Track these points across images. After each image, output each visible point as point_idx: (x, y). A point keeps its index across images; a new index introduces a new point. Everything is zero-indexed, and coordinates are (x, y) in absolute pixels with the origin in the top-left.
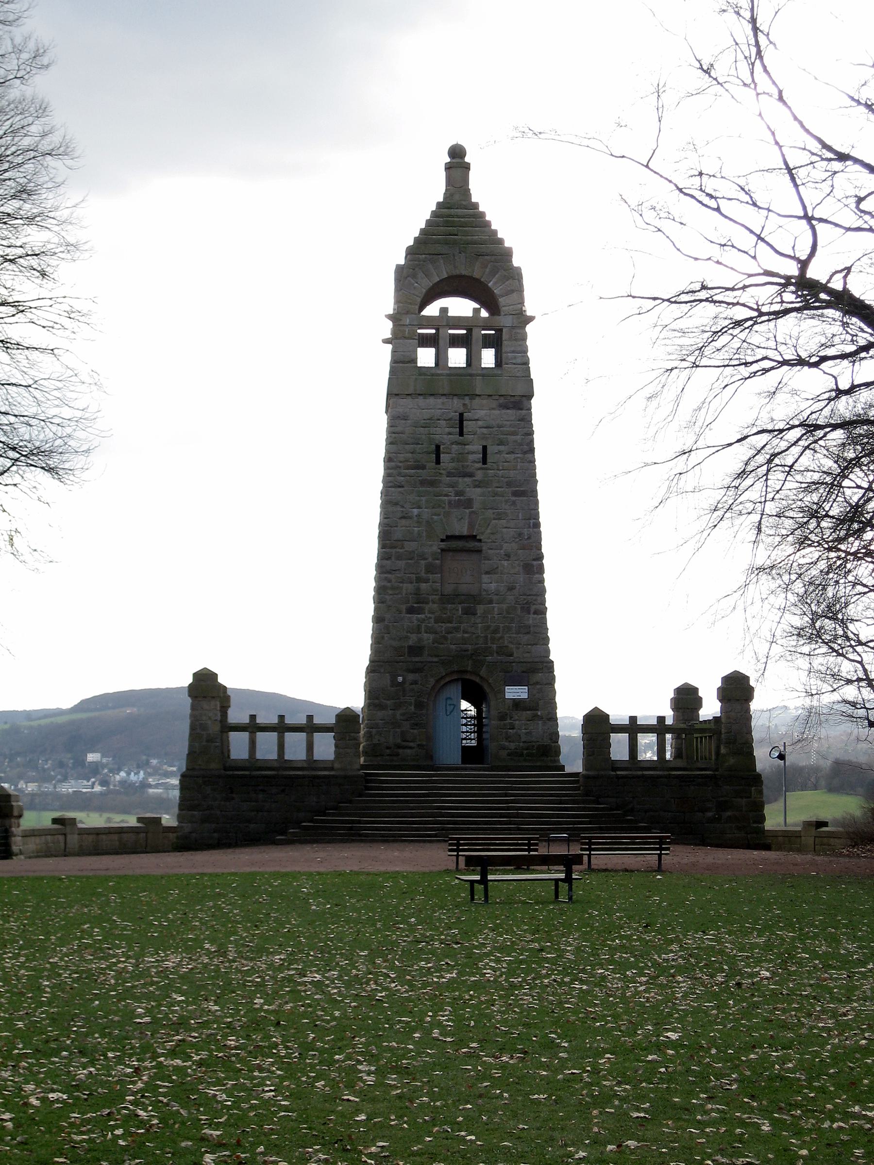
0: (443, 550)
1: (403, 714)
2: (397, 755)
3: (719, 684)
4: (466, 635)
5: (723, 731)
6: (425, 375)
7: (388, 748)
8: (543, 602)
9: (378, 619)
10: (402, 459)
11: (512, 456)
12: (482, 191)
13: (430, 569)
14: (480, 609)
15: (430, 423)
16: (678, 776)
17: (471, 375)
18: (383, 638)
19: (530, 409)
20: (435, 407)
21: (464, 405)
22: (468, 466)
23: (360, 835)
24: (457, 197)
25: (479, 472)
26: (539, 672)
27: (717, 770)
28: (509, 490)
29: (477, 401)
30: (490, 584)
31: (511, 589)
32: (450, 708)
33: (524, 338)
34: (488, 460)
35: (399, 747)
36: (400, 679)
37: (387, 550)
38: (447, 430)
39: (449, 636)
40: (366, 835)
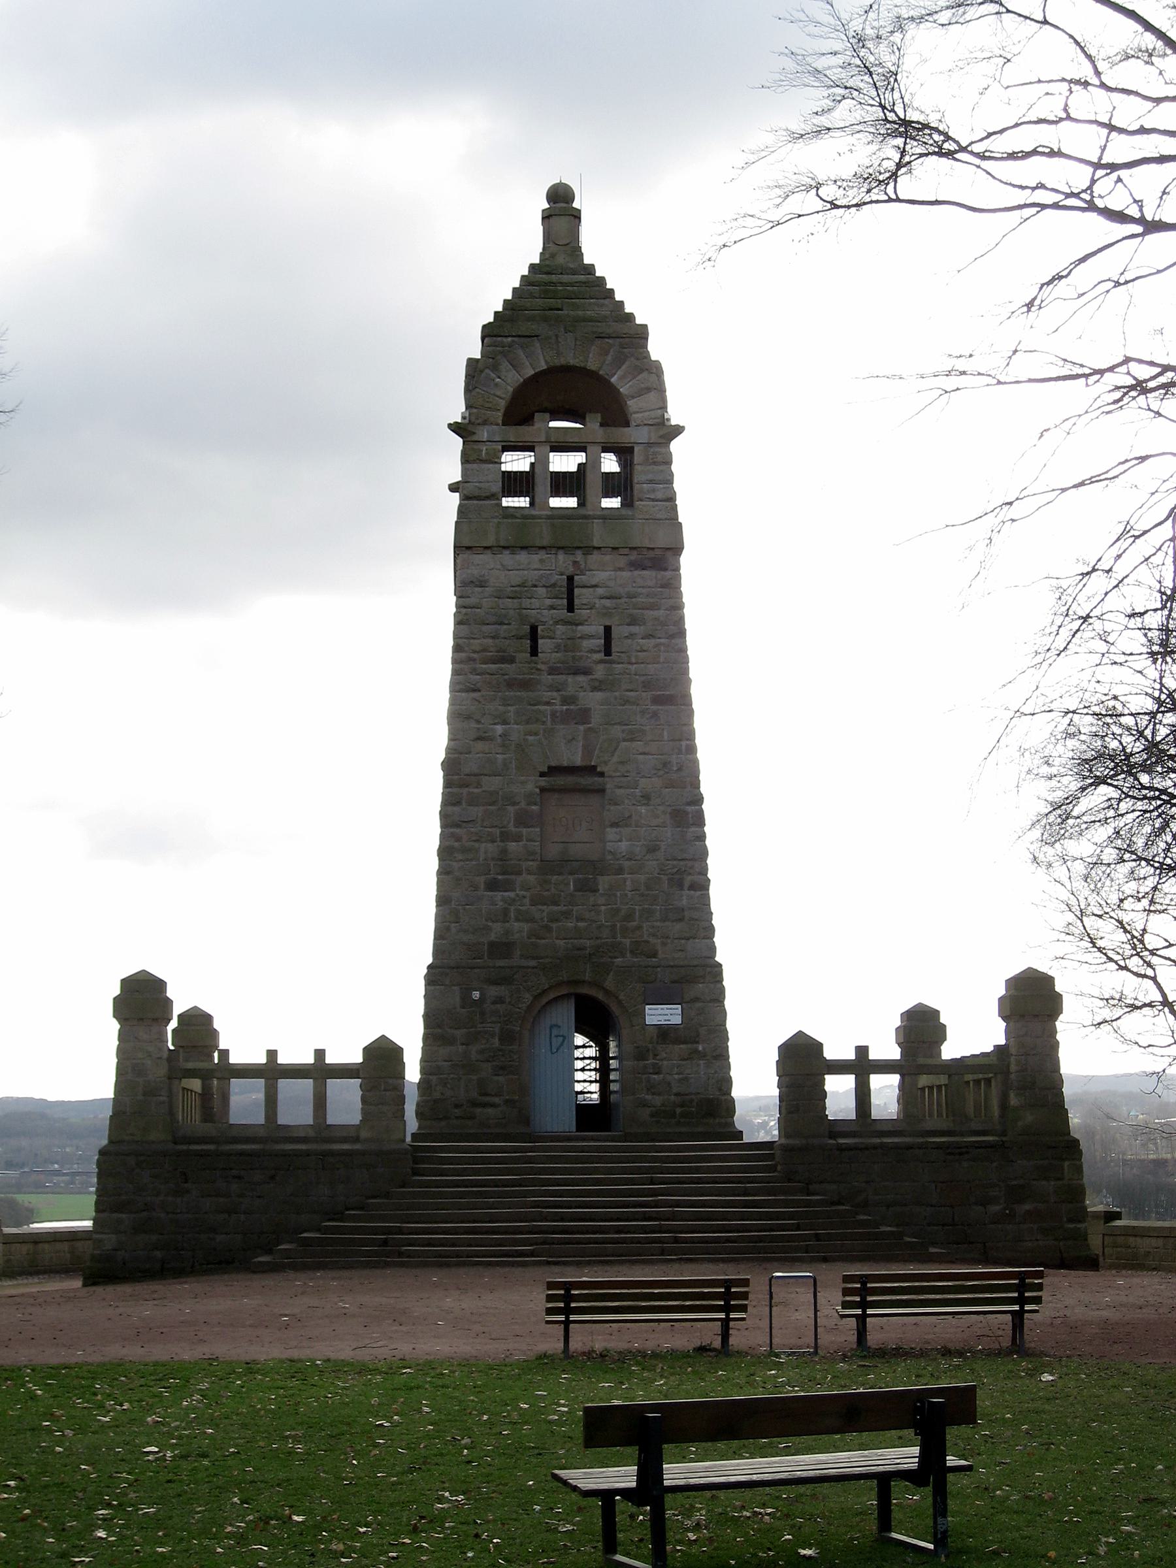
0: (543, 790)
1: (482, 1052)
2: (472, 1117)
3: (1002, 991)
4: (581, 924)
5: (1013, 1068)
6: (513, 517)
7: (457, 1106)
8: (704, 871)
9: (442, 900)
10: (478, 648)
11: (653, 641)
12: (597, 248)
13: (523, 820)
14: (603, 882)
15: (521, 590)
16: (939, 1146)
17: (585, 517)
18: (448, 929)
19: (678, 569)
20: (528, 566)
21: (575, 563)
22: (581, 657)
23: (400, 1254)
24: (561, 260)
25: (600, 667)
26: (699, 983)
27: (1004, 1133)
28: (647, 696)
29: (595, 557)
30: (620, 843)
31: (652, 849)
32: (556, 1042)
33: (668, 461)
34: (614, 649)
35: (475, 1104)
36: (476, 995)
37: (455, 790)
38: (548, 602)
39: (554, 925)
40: (409, 1255)
